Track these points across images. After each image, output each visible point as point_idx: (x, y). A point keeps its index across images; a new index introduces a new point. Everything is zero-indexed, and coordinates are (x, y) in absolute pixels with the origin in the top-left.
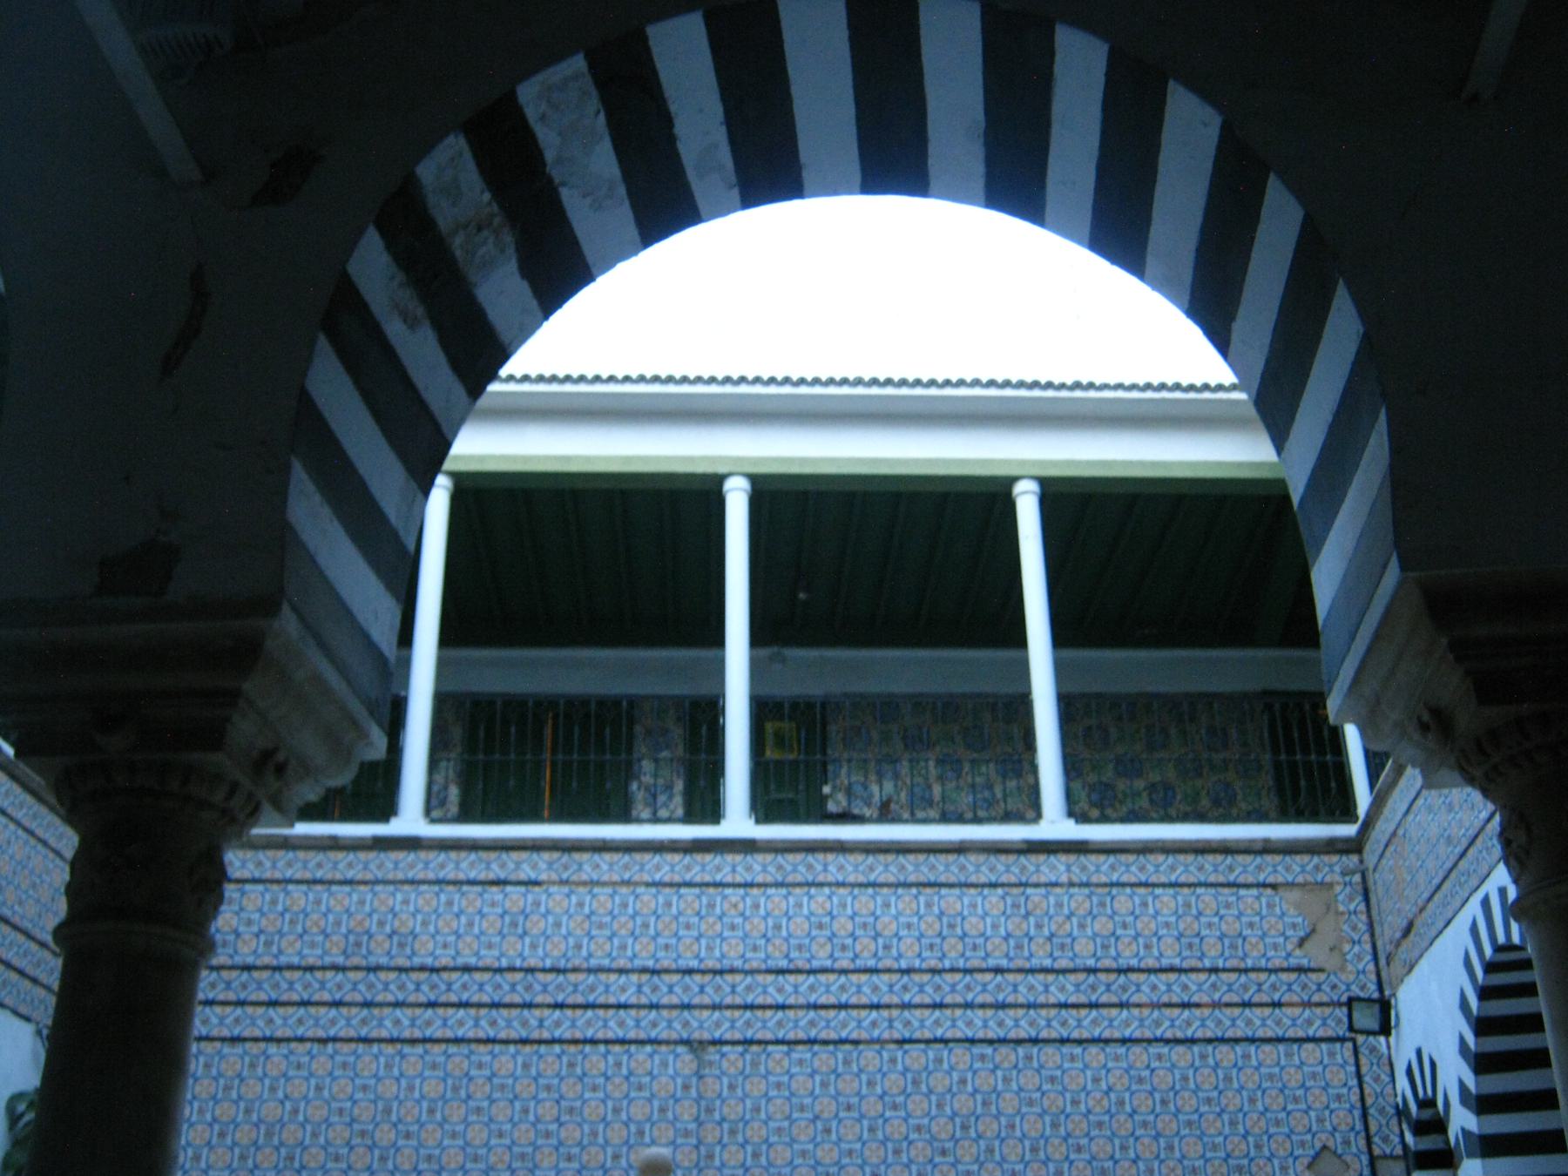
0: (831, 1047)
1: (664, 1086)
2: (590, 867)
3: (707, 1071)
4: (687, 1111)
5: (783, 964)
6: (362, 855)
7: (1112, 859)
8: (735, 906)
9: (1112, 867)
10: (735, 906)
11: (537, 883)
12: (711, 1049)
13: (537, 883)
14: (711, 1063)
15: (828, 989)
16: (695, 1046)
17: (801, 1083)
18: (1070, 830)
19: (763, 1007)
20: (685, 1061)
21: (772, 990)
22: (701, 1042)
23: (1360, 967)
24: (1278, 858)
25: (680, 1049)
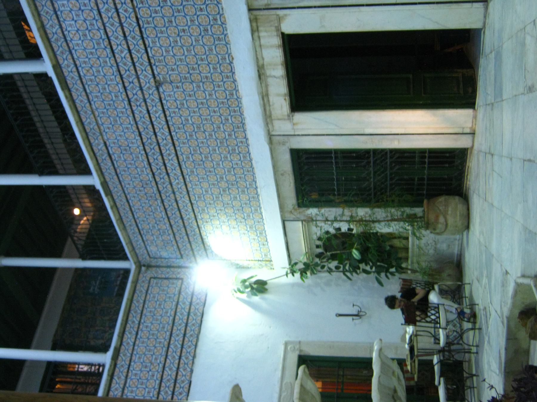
0: (143, 30)
1: (178, 94)
2: (91, 126)
3: (168, 79)
4: (188, 87)
5: (108, 50)
6: (115, 198)
7: (127, 333)
8: (88, 71)
9: (130, 333)
10: (88, 71)
11: (105, 144)
12: (158, 78)
13: (105, 144)
14: (164, 78)
15: (114, 31)
16: (158, 85)
17: (165, 42)
18: (110, 353)
19: (132, 58)
20: (165, 89)
21: (122, 54)
22: (155, 82)
23: (106, 6)
24: (117, 370)
25: (161, 90)
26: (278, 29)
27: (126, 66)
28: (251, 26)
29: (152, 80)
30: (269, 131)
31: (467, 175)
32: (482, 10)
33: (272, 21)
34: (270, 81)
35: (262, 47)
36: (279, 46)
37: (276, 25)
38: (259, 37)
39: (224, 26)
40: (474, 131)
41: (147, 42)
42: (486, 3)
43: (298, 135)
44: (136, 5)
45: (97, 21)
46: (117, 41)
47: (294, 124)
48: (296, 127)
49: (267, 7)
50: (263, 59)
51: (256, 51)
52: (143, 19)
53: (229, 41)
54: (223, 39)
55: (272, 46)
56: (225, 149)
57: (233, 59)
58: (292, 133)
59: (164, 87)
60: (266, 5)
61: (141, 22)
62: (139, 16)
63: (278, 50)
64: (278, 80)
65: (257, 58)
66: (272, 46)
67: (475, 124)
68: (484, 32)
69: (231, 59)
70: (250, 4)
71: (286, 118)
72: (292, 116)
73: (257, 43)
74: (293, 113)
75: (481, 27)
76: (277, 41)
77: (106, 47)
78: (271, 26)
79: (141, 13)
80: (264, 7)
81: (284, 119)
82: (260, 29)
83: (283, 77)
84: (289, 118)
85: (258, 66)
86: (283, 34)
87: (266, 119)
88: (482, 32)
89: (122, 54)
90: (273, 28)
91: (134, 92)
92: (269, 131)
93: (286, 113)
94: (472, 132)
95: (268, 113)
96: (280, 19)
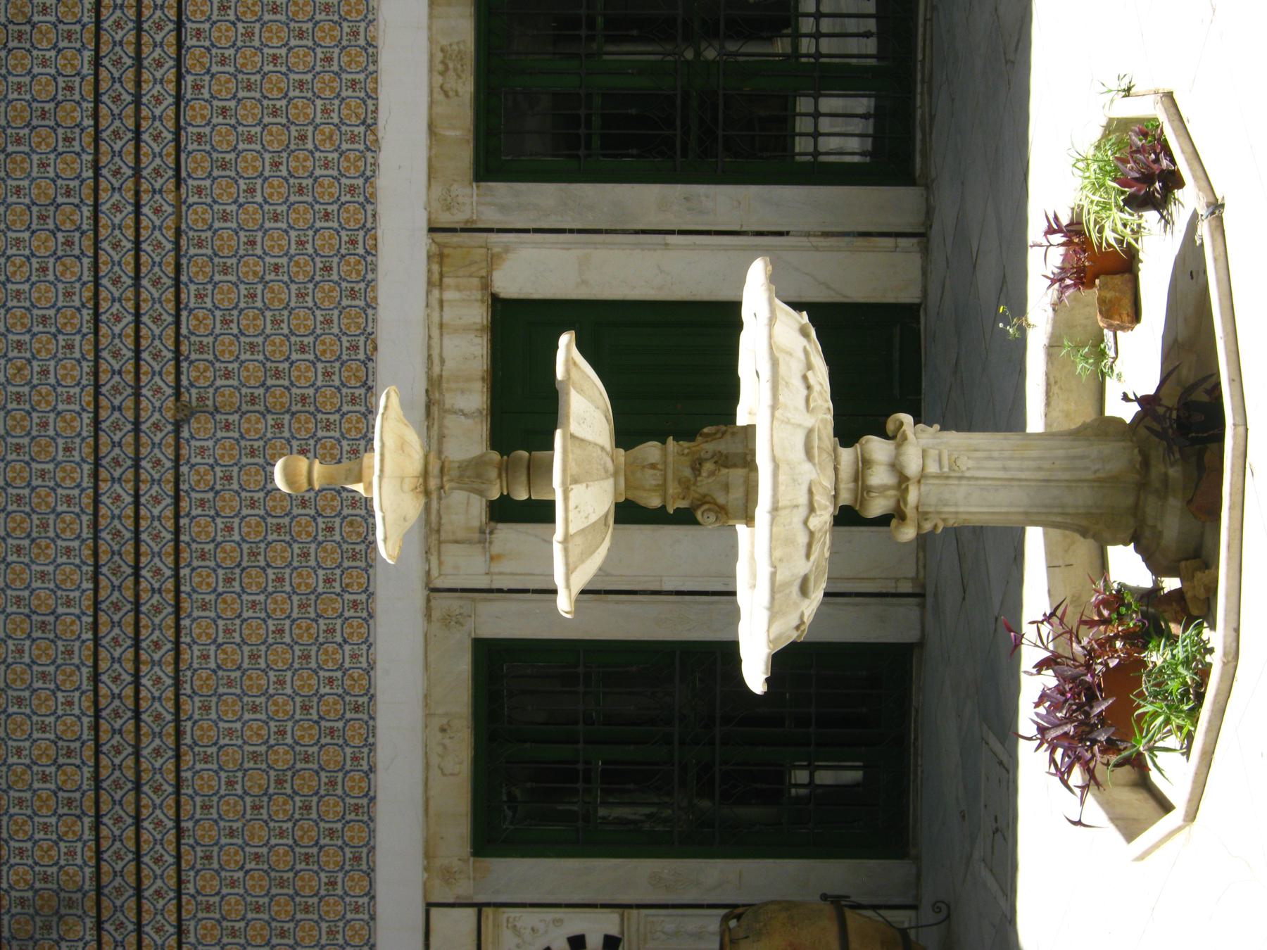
0: (184, 261)
3: (210, 403)
10: (20, 369)
12: (185, 397)
14: (201, 399)
20: (198, 427)
21: (118, 328)
25: (185, 434)
26: (486, 283)
27: (117, 362)
28: (429, 271)
29: (170, 403)
30: (428, 573)
31: (916, 739)
32: (916, 259)
33: (473, 263)
34: (451, 422)
35: (445, 304)
36: (482, 301)
37: (483, 273)
38: (441, 302)
39: (369, 258)
40: (923, 586)
41: (184, 296)
42: (924, 239)
43: (500, 591)
44: (184, 197)
45: (83, 233)
46: (116, 308)
47: (492, 558)
48: (496, 568)
49: (469, 226)
50: (442, 361)
51: (430, 337)
52: (191, 234)
53: (375, 298)
54: (361, 295)
55: (466, 329)
56: (308, 629)
57: (375, 348)
58: (483, 583)
59: (194, 424)
60: (467, 222)
61: (183, 242)
62: (183, 226)
63: (478, 340)
64: (469, 422)
65: (429, 357)
66: (466, 329)
67: (925, 567)
68: (925, 310)
69: (370, 347)
70: (433, 216)
71: (476, 536)
72: (491, 533)
73: (436, 317)
74: (493, 524)
75: (917, 301)
76: (479, 314)
77: (83, 305)
78: (471, 276)
79: (191, 217)
80: (462, 226)
81: (469, 542)
82: (446, 280)
83: (481, 413)
84: (483, 538)
85: (430, 379)
86: (495, 298)
87: (427, 537)
88: (922, 312)
89: (118, 328)
90: (476, 282)
91: (117, 434)
92: (428, 573)
93: (476, 524)
94: (918, 590)
95: (434, 517)
96: (493, 260)
